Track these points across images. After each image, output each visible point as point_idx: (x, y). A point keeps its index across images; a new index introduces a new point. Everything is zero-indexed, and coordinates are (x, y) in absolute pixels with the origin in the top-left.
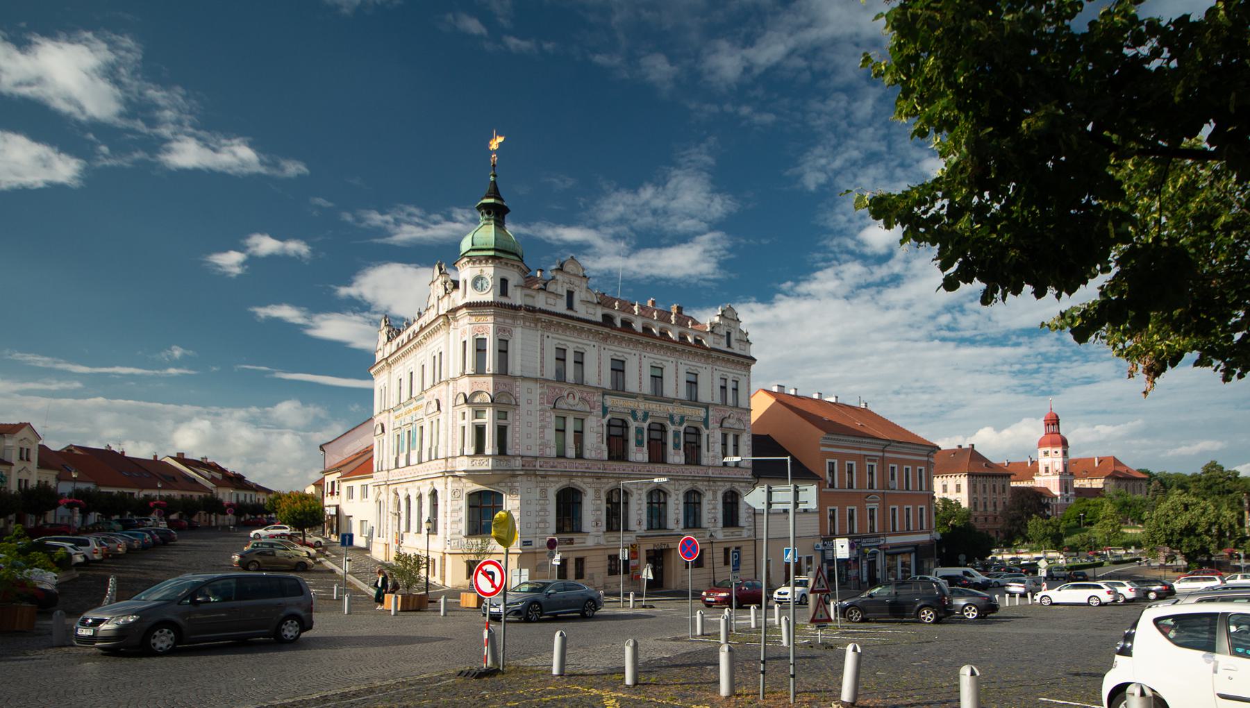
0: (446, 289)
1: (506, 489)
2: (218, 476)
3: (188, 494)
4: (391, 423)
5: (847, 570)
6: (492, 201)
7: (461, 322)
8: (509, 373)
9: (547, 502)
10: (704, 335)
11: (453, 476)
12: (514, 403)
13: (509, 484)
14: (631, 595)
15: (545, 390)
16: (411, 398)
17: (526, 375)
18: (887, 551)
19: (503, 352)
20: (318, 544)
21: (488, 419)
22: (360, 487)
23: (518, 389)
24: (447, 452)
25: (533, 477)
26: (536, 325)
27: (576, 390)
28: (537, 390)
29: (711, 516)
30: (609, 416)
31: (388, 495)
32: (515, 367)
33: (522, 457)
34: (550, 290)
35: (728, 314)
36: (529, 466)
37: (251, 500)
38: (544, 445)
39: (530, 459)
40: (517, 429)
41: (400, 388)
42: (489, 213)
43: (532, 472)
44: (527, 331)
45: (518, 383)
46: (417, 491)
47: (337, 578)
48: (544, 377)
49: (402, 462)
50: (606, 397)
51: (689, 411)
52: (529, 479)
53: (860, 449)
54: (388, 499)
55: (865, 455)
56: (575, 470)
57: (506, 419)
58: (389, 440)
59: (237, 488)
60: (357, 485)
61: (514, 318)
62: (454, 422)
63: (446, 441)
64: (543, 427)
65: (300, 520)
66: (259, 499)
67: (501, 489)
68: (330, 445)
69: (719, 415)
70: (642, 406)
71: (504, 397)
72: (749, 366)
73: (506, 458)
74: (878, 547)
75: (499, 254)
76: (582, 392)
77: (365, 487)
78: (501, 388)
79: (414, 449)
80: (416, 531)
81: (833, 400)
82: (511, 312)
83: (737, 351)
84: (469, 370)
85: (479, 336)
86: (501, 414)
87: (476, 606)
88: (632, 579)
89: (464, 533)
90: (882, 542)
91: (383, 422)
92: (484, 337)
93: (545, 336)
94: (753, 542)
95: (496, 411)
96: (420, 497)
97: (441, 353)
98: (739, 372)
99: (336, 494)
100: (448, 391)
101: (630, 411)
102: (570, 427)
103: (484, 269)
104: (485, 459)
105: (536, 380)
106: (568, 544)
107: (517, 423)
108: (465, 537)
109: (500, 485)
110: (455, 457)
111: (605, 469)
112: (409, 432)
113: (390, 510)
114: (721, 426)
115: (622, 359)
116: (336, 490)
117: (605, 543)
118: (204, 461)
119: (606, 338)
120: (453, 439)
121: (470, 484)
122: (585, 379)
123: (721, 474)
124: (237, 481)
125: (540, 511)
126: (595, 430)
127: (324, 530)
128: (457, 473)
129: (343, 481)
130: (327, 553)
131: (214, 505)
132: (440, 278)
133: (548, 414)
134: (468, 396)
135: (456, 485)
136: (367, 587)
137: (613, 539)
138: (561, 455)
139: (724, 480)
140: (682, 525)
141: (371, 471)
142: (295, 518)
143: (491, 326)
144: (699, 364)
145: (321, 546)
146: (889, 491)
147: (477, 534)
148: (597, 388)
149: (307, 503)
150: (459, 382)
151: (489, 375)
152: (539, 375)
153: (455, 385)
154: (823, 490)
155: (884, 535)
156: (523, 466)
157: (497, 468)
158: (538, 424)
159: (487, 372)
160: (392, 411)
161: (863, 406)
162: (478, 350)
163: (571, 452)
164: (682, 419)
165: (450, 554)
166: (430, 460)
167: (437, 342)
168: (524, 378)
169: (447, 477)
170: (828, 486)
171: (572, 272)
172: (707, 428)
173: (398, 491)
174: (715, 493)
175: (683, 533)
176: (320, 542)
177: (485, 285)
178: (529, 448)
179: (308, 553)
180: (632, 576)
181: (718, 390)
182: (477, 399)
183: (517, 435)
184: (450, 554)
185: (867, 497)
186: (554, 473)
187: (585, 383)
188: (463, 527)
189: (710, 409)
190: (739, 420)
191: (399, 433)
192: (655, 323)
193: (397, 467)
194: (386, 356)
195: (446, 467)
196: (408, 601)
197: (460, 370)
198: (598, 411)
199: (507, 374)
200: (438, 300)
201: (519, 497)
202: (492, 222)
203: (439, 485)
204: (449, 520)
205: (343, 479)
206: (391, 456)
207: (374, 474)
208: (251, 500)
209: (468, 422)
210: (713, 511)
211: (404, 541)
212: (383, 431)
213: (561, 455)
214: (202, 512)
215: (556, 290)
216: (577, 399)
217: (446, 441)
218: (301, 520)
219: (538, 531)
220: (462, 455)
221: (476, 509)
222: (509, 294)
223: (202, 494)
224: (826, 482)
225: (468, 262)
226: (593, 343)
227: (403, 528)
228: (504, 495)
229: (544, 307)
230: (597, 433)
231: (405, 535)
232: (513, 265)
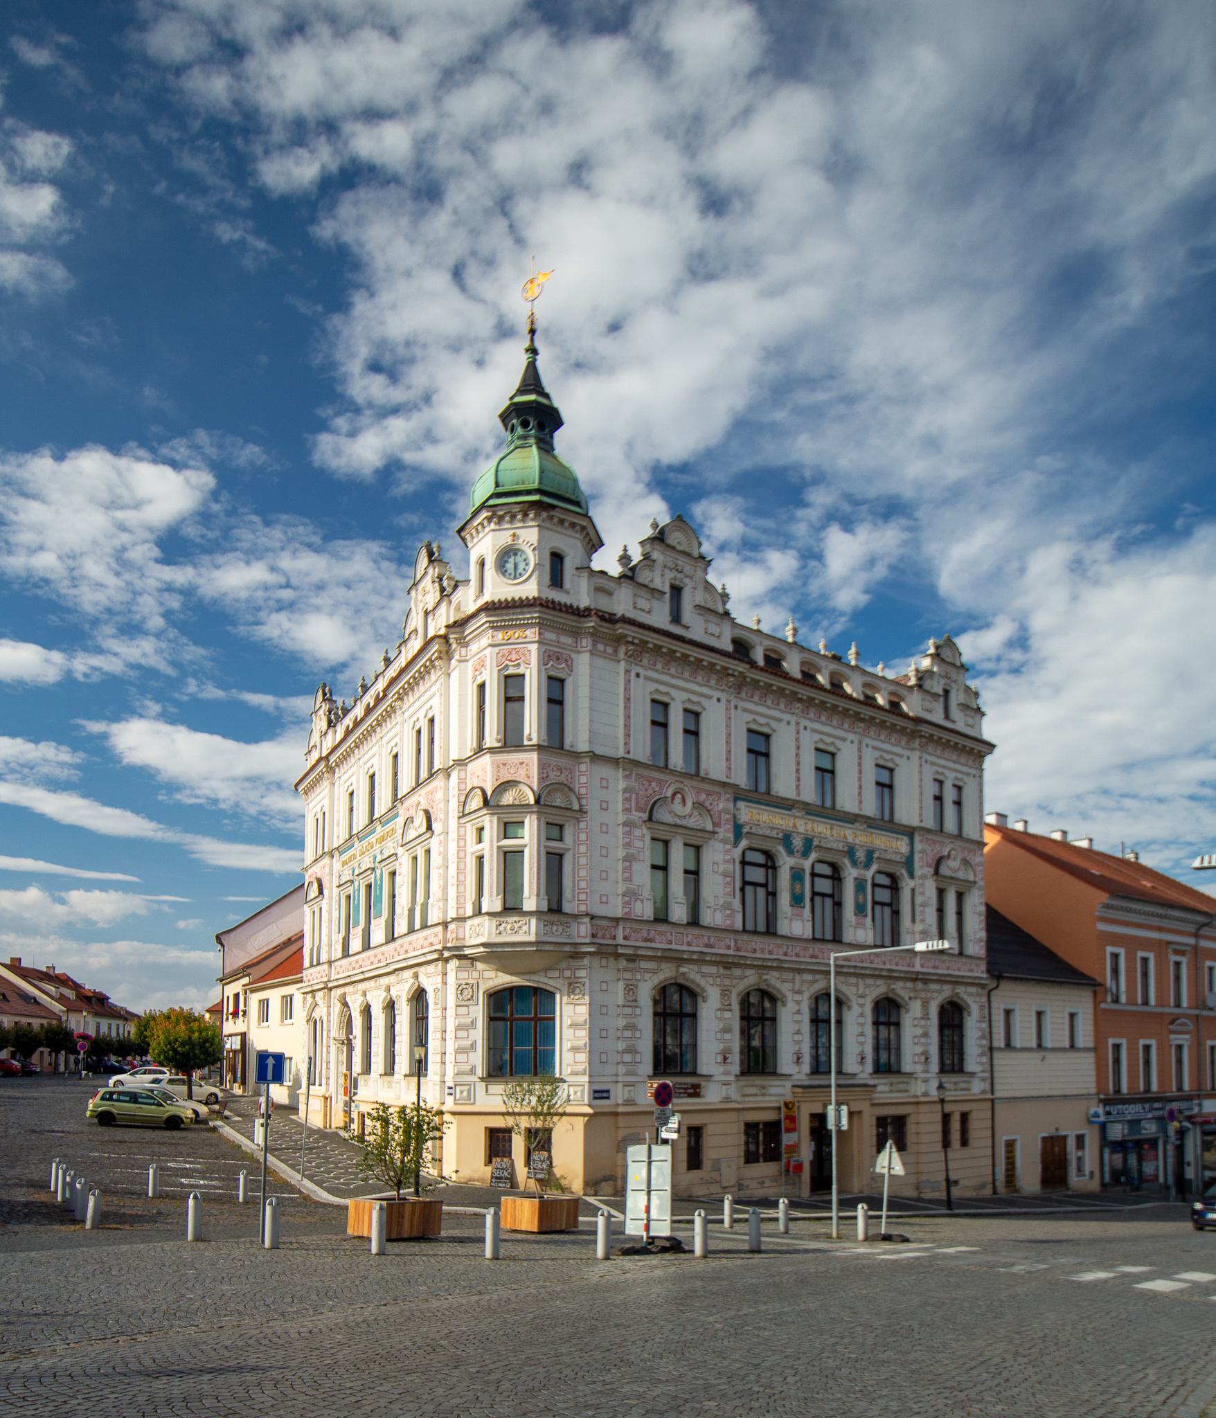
0: (442, 590)
2: (70, 994)
3: (24, 1020)
7: (474, 647)
8: (567, 747)
10: (904, 692)
12: (576, 807)
13: (567, 973)
14: (781, 1206)
15: (633, 783)
16: (372, 821)
18: (1207, 1127)
19: (555, 700)
20: (213, 1098)
21: (529, 835)
22: (279, 999)
23: (583, 779)
24: (446, 911)
25: (611, 959)
26: (616, 651)
27: (688, 786)
28: (619, 781)
29: (919, 1049)
30: (744, 843)
31: (329, 1007)
32: (579, 736)
33: (593, 917)
34: (641, 580)
35: (946, 654)
36: (604, 937)
37: (118, 1034)
38: (631, 895)
39: (605, 923)
40: (583, 861)
41: (351, 810)
42: (525, 424)
43: (610, 950)
44: (600, 662)
45: (583, 767)
46: (385, 994)
47: (243, 1159)
48: (631, 756)
50: (741, 804)
51: (880, 840)
52: (604, 962)
53: (1160, 929)
54: (329, 1014)
55: (1169, 943)
56: (685, 948)
57: (561, 840)
58: (331, 905)
60: (275, 996)
61: (576, 633)
62: (461, 849)
63: (445, 889)
64: (629, 859)
65: (183, 1054)
66: (129, 1032)
67: (551, 982)
68: (232, 935)
69: (933, 851)
70: (802, 826)
71: (558, 795)
72: (980, 757)
73: (563, 919)
74: (1190, 1118)
75: (545, 499)
76: (699, 791)
77: (288, 1001)
78: (554, 776)
81: (1084, 844)
82: (571, 621)
84: (491, 740)
85: (511, 671)
86: (553, 830)
87: (536, 1230)
88: (788, 1171)
89: (480, 1072)
90: (1196, 1110)
91: (319, 875)
92: (520, 671)
93: (633, 674)
94: (989, 1104)
95: (543, 820)
96: (390, 1006)
97: (432, 721)
98: (965, 769)
99: (241, 1014)
100: (447, 789)
101: (780, 835)
102: (679, 858)
103: (518, 532)
104: (524, 920)
105: (615, 762)
106: (690, 1095)
107: (583, 849)
108: (482, 1079)
109: (550, 974)
110: (461, 919)
112: (369, 886)
113: (334, 1034)
114: (937, 872)
115: (765, 730)
116: (241, 1007)
117: (739, 1099)
118: (51, 973)
119: (741, 684)
121: (491, 974)
122: (703, 766)
123: (935, 967)
124: (97, 1003)
125: (626, 1028)
126: (721, 869)
127: (222, 1078)
128: (467, 951)
129: (253, 991)
130: (227, 1113)
131: (59, 1039)
132: (430, 571)
133: (638, 832)
134: (489, 794)
135: (464, 975)
136: (299, 1177)
137: (753, 1090)
138: (662, 918)
139: (941, 980)
140: (869, 1068)
141: (299, 968)
142: (175, 1051)
143: (534, 648)
144: (897, 750)
145: (217, 1102)
147: (503, 1075)
148: (724, 785)
149: (195, 1025)
151: (531, 748)
152: (621, 753)
154: (1103, 1006)
155: (1198, 1097)
156: (593, 936)
157: (545, 939)
158: (621, 853)
159: (526, 743)
160: (336, 854)
161: (1131, 857)
162: (508, 699)
163: (679, 913)
164: (870, 853)
165: (454, 1114)
166: (411, 931)
167: (423, 700)
168: (595, 757)
169: (447, 960)
170: (1109, 999)
171: (679, 548)
172: (912, 876)
173: (348, 999)
174: (925, 1004)
176: (216, 1096)
177: (521, 566)
178: (604, 901)
179: (195, 1112)
180: (788, 1164)
181: (929, 803)
182: (508, 798)
183: (583, 873)
184: (454, 1114)
185: (1172, 1023)
186: (650, 953)
187: (702, 774)
188: (478, 1059)
189: (917, 838)
190: (966, 862)
191: (350, 890)
193: (346, 953)
195: (445, 940)
196: (401, 1216)
197: (471, 743)
198: (726, 832)
199: (562, 748)
200: (427, 613)
201: (587, 999)
202: (532, 441)
203: (430, 979)
204: (451, 1046)
205: (250, 989)
206: (334, 937)
207: (305, 973)
208: (118, 1034)
209: (489, 847)
210: (923, 1040)
211: (359, 1091)
212: (321, 892)
213: (662, 918)
214: (46, 1050)
215: (652, 581)
217: (445, 889)
218: (185, 1055)
219: (622, 1069)
220: (478, 912)
221: (501, 1023)
222: (567, 583)
223: (45, 1022)
225: (489, 519)
226: (717, 694)
227: (357, 1067)
228: (558, 997)
229: (631, 614)
230: (725, 875)
232: (573, 525)
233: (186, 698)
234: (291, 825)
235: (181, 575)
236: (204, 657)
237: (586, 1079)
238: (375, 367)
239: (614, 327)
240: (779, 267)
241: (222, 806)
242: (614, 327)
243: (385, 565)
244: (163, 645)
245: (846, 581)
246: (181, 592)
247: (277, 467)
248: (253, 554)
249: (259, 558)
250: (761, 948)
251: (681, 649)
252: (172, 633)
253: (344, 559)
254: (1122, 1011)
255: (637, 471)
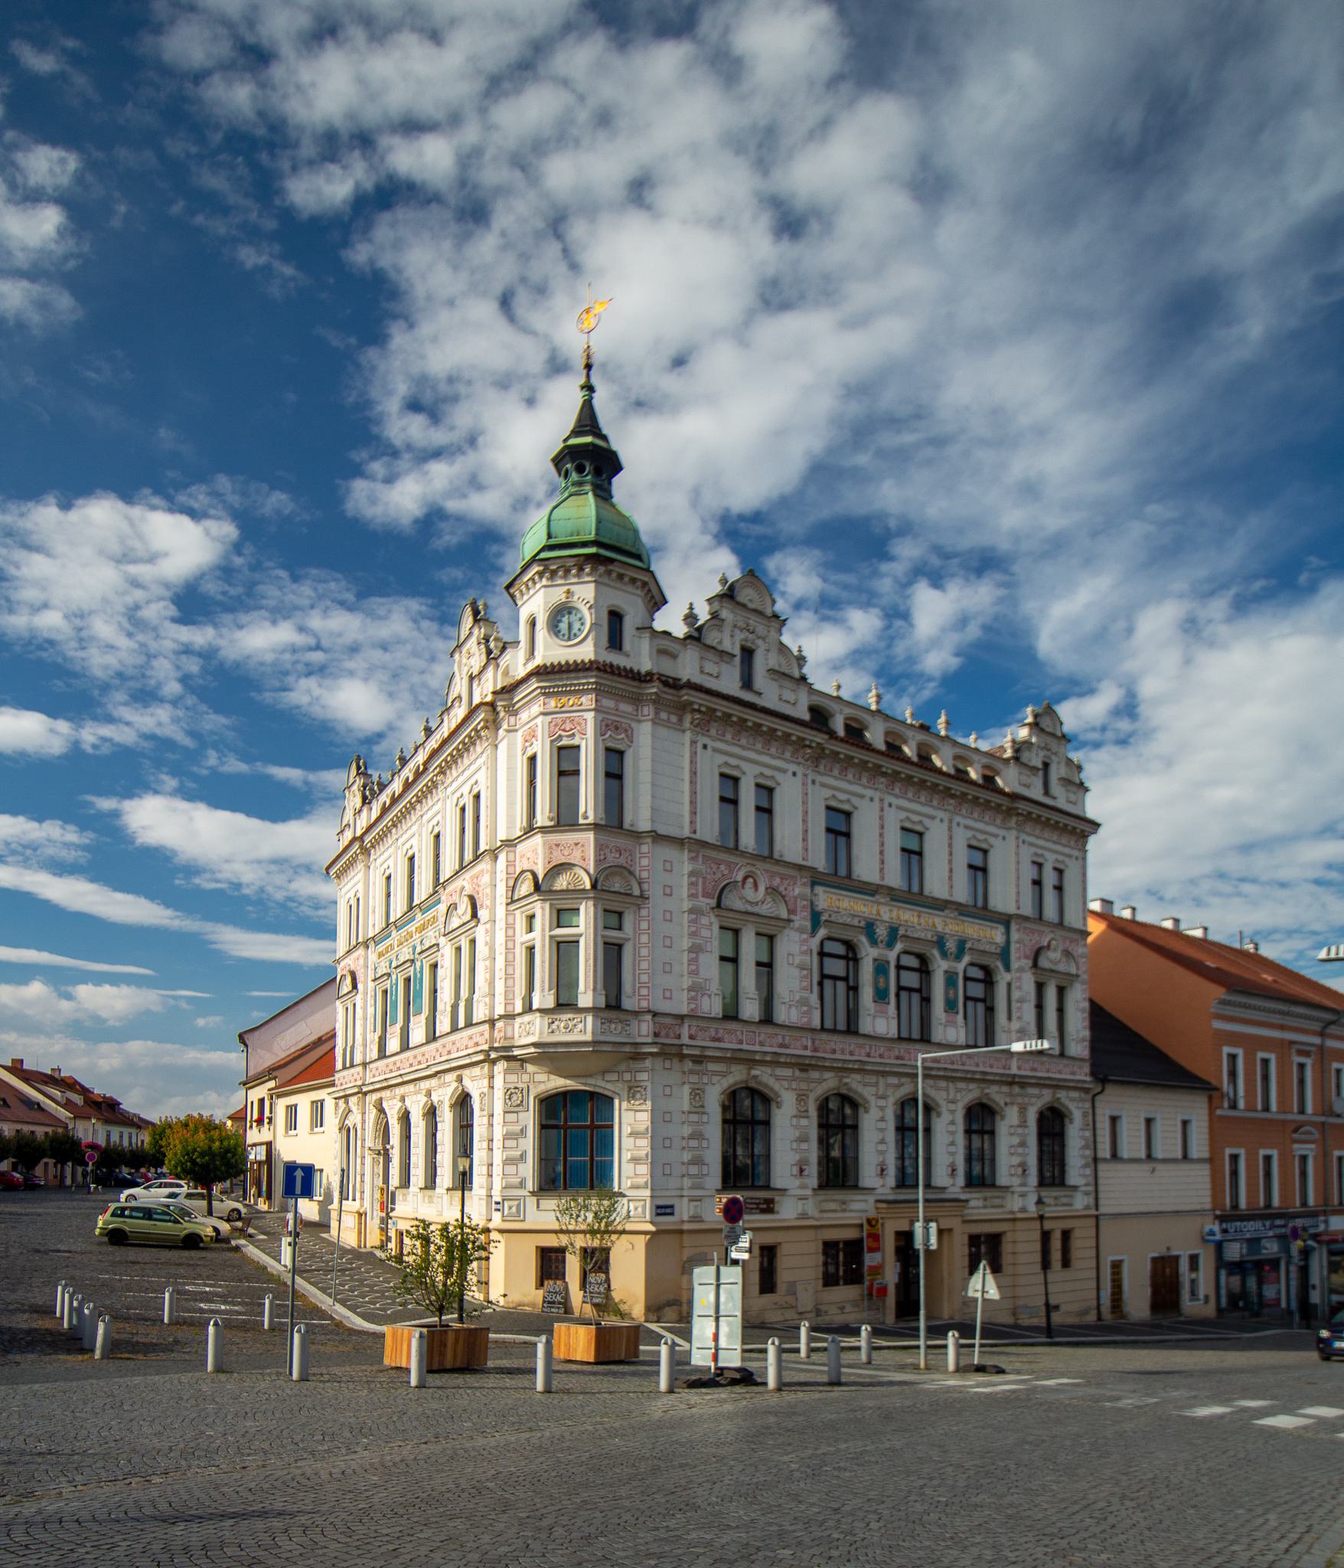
0: (489, 652)
1: (619, 1087)
2: (78, 1099)
4: (371, 967)
5: (1260, 1283)
6: (588, 439)
7: (524, 716)
8: (626, 825)
9: (705, 1118)
11: (509, 1059)
12: (637, 892)
13: (627, 1076)
14: (864, 1334)
15: (700, 866)
16: (411, 908)
17: (662, 830)
18: (1334, 1247)
19: (614, 773)
20: (235, 1215)
21: (585, 923)
23: (645, 862)
24: (492, 1008)
25: (676, 1061)
26: (681, 720)
28: (684, 864)
29: (1016, 1160)
30: (822, 932)
31: (364, 1114)
32: (640, 814)
33: (655, 1014)
34: (709, 642)
35: (1046, 723)
36: (667, 1036)
37: (130, 1143)
39: (668, 1021)
40: (644, 952)
41: (388, 895)
42: (580, 469)
43: (674, 1050)
44: (663, 732)
45: (645, 848)
46: (425, 1099)
47: (269, 1281)
48: (697, 836)
49: (393, 1045)
50: (819, 890)
52: (668, 1064)
53: (1282, 1027)
54: (363, 1122)
56: (757, 1048)
57: (620, 928)
59: (107, 1121)
60: (303, 1102)
61: (637, 700)
62: (510, 939)
63: (492, 984)
66: (143, 1142)
67: (609, 1086)
68: (257, 1033)
70: (887, 913)
71: (617, 879)
72: (1083, 837)
73: (622, 1016)
76: (773, 875)
77: (318, 1107)
78: (612, 858)
79: (419, 1013)
80: (422, 1184)
81: (1198, 933)
82: (631, 686)
83: (1061, 803)
84: (542, 818)
85: (565, 742)
86: (612, 918)
88: (870, 1294)
89: (530, 1185)
90: (1322, 1227)
92: (575, 742)
93: (699, 746)
94: (1093, 1221)
96: (431, 1113)
97: (477, 797)
98: (1067, 850)
99: (266, 1121)
100: (494, 873)
101: (863, 924)
102: (750, 949)
103: (573, 588)
104: (579, 1017)
105: (679, 842)
107: (644, 939)
108: (533, 1193)
109: (608, 1077)
110: (509, 1017)
111: (815, 1050)
113: (369, 1143)
114: (1035, 965)
115: (846, 807)
116: (267, 1113)
117: (817, 1215)
118: (56, 1075)
119: (818, 756)
120: (509, 976)
121: (543, 1077)
124: (108, 1109)
125: (692, 1137)
126: (797, 961)
127: (245, 1192)
128: (516, 1052)
129: (279, 1096)
130: (251, 1231)
131: (66, 1148)
133: (705, 921)
134: (540, 877)
135: (513, 1078)
136: (330, 1301)
137: (832, 1206)
138: (731, 1015)
139: (1042, 1084)
140: (961, 1180)
141: (331, 1071)
142: (194, 1162)
143: (590, 716)
144: (992, 829)
145: (240, 1219)
146: (1332, 1120)
147: (556, 1189)
148: (800, 868)
149: (215, 1134)
150: (520, 848)
151: (587, 828)
152: (686, 832)
153: (511, 857)
154: (1219, 1112)
155: (1325, 1213)
156: (656, 1035)
157: (602, 1038)
158: (686, 943)
159: (581, 821)
160: (372, 944)
161: (1250, 947)
162: (561, 773)
163: (750, 1009)
164: (961, 944)
165: (501, 1231)
166: (455, 1029)
167: (467, 773)
168: (657, 837)
169: (494, 1062)
170: (1226, 1105)
171: (751, 606)
172: (1008, 968)
173: (385, 1105)
174: (1023, 1110)
175: (963, 1197)
176: (239, 1211)
177: (576, 626)
179: (216, 1229)
180: (871, 1287)
181: (1027, 889)
182: (562, 882)
183: (644, 965)
184: (501, 1231)
186: (718, 1054)
187: (776, 856)
189: (1014, 927)
190: (1067, 953)
191: (387, 984)
192: (909, 733)
193: (382, 1054)
194: (359, 833)
195: (492, 1039)
196: (444, 1345)
197: (520, 821)
198: (802, 920)
201: (649, 1105)
202: (588, 488)
203: (475, 1084)
205: (276, 1094)
207: (337, 1076)
208: (130, 1143)
209: (540, 937)
210: (1020, 1150)
211: (397, 1207)
213: (731, 1015)
214: (51, 1161)
215: (720, 642)
216: (762, 889)
217: (492, 984)
218: (205, 1167)
219: (687, 1182)
220: (528, 1009)
221: (554, 1131)
222: (627, 645)
223: (49, 1130)
224: (1222, 1096)
225: (541, 574)
226: (793, 768)
227: (395, 1181)
228: (616, 1102)
229: (698, 679)
230: (802, 968)
231: (399, 1195)
232: (633, 581)
233: (205, 772)
234: (321, 912)
235: (200, 636)
236: (227, 727)
237: (647, 1193)
238: (414, 406)
239: (679, 362)
240: (861, 295)
241: (246, 891)
242: (679, 362)
243: (426, 624)
244: (180, 713)
245: (935, 643)
246: (200, 655)
247: (307, 517)
248: (279, 613)
249: (286, 618)
250: (841, 1048)
251: (753, 717)
252: (191, 700)
253: (381, 618)
254: (1240, 1118)
255: (704, 521)
